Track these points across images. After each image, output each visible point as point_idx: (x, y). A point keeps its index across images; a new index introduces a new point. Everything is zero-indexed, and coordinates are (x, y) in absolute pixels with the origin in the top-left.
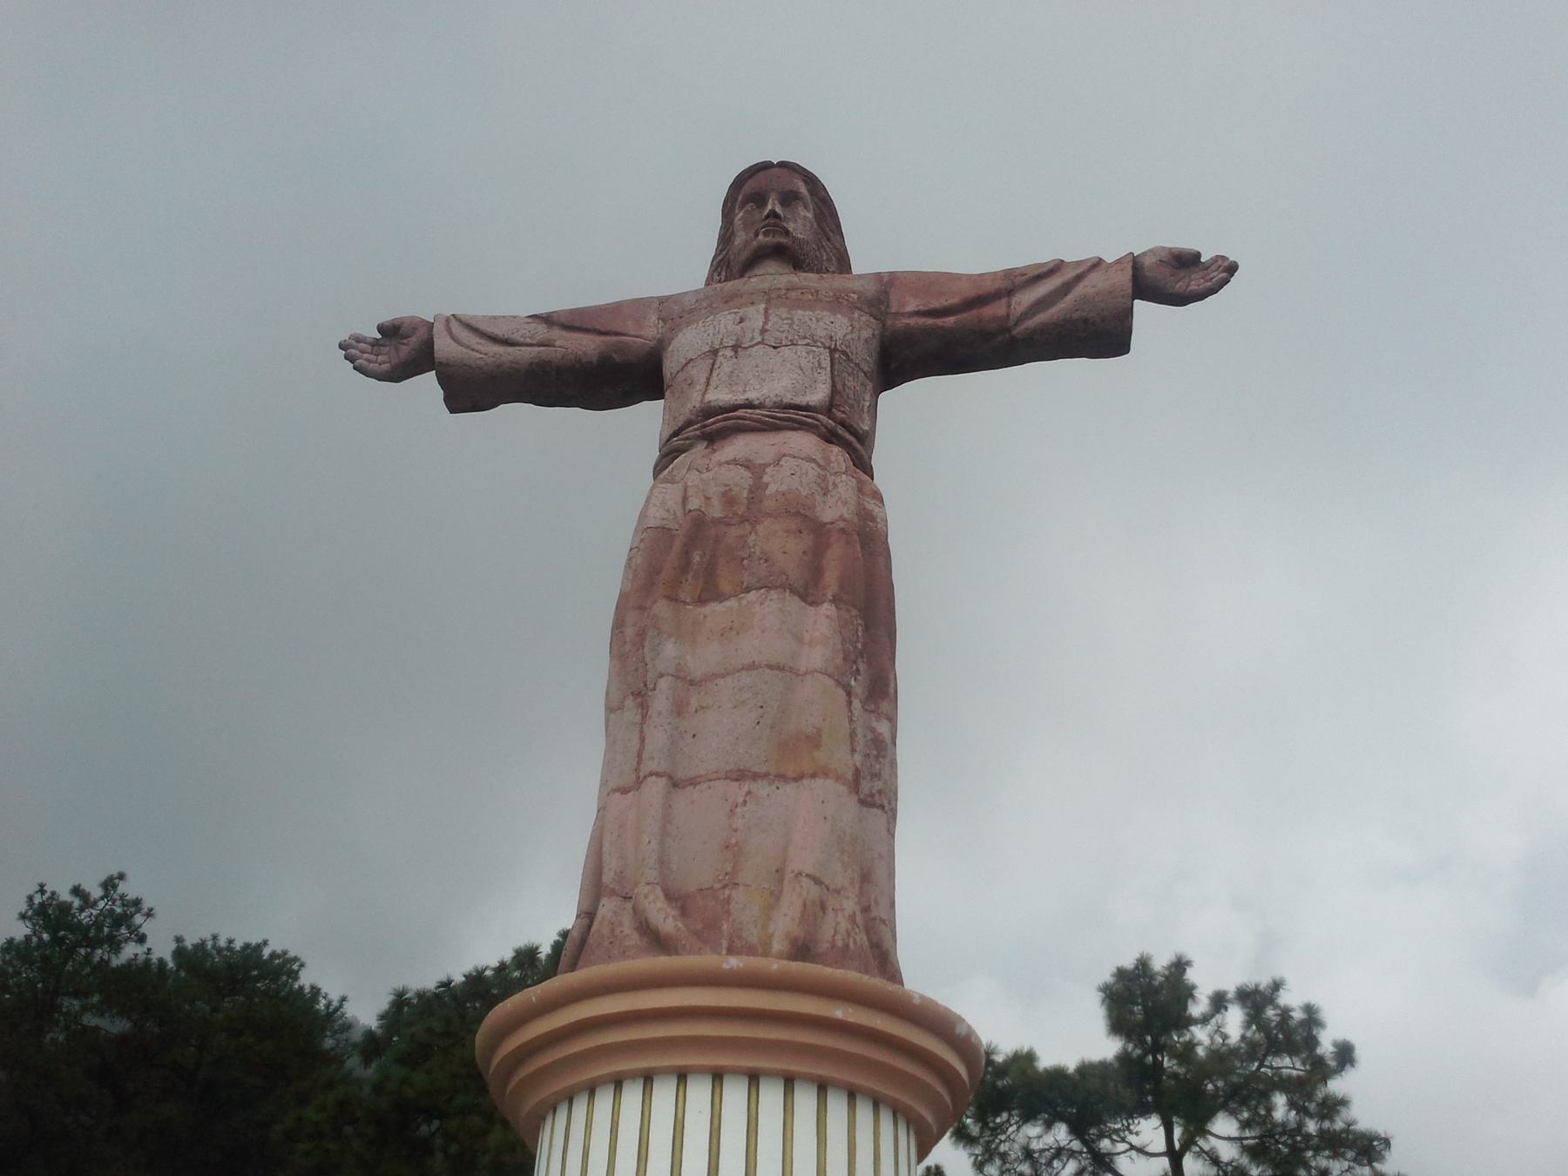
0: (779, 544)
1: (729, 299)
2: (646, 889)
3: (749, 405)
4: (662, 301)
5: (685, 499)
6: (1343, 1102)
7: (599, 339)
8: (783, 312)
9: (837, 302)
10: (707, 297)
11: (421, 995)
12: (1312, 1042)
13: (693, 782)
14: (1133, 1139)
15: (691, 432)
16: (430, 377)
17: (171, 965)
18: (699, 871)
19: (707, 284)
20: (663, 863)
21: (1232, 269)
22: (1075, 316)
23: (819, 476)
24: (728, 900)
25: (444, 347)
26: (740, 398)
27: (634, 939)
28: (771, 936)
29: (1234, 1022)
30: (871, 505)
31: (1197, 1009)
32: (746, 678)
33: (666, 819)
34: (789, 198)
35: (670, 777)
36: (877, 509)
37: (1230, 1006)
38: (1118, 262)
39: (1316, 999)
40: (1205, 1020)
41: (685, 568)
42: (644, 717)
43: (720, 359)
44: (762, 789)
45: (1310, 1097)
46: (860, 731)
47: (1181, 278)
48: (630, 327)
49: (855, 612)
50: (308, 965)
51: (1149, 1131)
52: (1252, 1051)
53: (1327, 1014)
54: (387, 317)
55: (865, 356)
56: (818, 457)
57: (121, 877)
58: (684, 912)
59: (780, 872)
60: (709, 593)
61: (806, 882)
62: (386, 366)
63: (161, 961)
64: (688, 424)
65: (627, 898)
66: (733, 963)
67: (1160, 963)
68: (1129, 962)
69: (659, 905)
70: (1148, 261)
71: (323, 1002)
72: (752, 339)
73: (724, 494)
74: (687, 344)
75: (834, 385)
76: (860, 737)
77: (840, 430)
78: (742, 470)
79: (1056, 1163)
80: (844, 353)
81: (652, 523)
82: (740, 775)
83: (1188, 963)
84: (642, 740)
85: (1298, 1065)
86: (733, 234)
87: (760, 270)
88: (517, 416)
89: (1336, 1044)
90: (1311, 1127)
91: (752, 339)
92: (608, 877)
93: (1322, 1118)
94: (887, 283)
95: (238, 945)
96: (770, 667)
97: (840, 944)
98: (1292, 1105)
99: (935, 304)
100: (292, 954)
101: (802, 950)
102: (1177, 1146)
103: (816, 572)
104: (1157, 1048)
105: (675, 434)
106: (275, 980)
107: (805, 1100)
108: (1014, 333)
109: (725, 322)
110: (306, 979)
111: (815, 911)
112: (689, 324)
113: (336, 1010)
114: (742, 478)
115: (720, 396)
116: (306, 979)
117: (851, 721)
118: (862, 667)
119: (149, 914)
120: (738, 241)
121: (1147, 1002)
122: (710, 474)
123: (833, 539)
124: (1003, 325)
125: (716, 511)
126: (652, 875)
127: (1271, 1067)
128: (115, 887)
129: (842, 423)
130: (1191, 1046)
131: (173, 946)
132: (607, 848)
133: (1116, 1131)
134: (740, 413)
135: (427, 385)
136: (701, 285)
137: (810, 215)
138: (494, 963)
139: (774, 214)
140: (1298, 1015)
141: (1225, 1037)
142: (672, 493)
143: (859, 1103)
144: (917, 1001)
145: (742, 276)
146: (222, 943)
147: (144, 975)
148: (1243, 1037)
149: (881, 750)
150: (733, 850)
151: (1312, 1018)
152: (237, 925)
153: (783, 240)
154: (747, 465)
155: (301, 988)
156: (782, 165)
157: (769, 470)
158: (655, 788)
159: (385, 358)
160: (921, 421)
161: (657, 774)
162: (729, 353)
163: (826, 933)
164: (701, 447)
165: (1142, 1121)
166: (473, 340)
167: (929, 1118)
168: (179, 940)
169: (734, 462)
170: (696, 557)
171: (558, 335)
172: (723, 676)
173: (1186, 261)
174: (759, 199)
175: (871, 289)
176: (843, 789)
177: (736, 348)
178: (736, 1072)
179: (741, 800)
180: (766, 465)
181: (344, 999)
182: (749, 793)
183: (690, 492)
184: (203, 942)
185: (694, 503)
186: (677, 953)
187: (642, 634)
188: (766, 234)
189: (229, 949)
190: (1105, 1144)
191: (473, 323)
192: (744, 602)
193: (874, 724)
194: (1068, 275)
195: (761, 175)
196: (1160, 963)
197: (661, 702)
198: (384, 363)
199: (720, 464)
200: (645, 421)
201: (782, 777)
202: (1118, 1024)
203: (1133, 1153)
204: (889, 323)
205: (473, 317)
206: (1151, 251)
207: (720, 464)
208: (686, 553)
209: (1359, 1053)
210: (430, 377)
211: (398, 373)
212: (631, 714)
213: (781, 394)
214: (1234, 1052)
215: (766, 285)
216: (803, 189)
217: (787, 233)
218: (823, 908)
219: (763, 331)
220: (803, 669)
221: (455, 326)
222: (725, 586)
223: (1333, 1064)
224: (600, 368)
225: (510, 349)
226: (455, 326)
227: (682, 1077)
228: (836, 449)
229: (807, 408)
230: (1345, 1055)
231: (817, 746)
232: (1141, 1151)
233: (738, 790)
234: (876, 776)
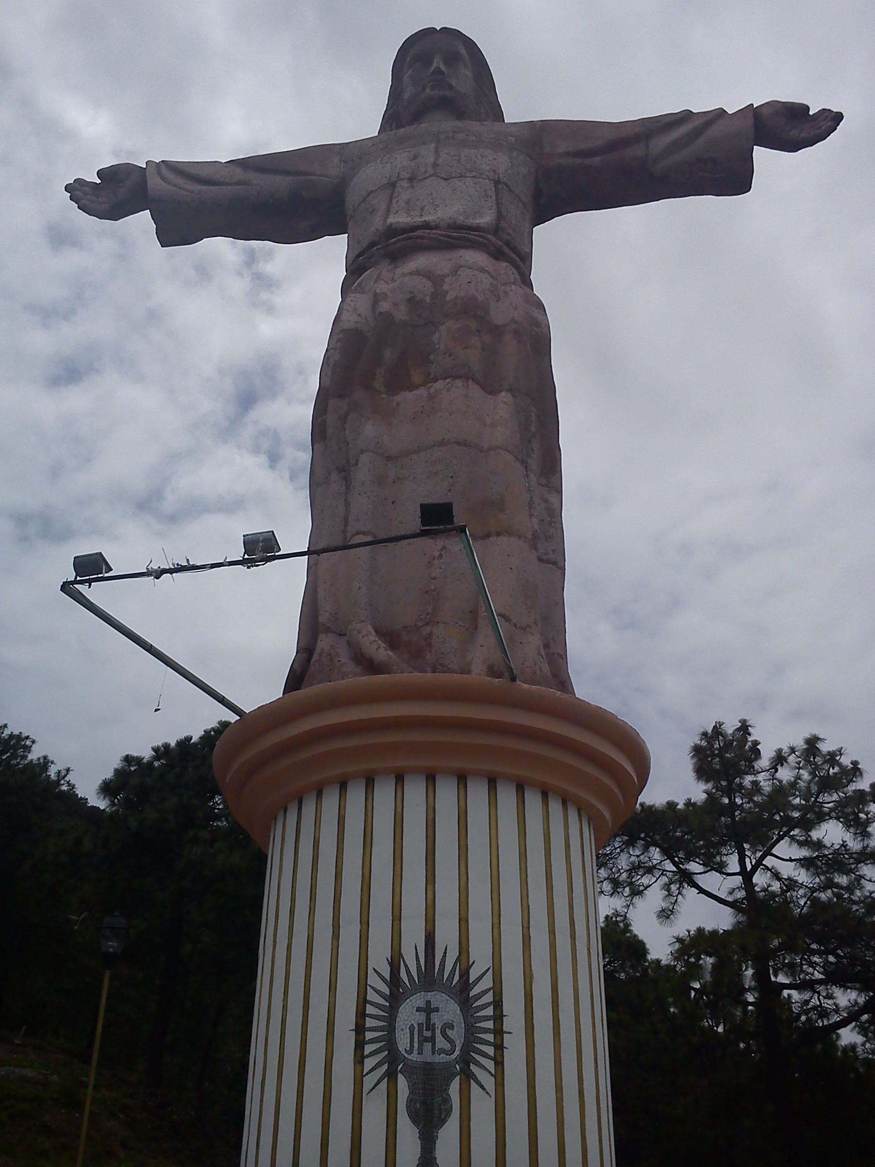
2: (359, 626)
3: (426, 226)
21: (838, 118)
23: (491, 285)
24: (431, 634)
25: (154, 183)
26: (418, 220)
27: (351, 667)
30: (536, 313)
31: (764, 762)
34: (452, 58)
36: (541, 318)
47: (795, 126)
64: (372, 244)
65: (341, 635)
67: (730, 727)
69: (372, 638)
72: (426, 172)
77: (506, 250)
78: (424, 280)
81: (346, 326)
92: (323, 618)
94: (540, 133)
96: (458, 443)
99: (583, 146)
100: (25, 734)
102: (749, 867)
104: (729, 792)
105: (358, 256)
107: (507, 797)
109: (401, 160)
115: (400, 219)
120: (406, 96)
121: (723, 755)
125: (402, 314)
129: (508, 244)
132: (321, 593)
134: (419, 233)
137: (469, 74)
139: (438, 71)
142: (362, 302)
162: (405, 184)
166: (181, 181)
171: (251, 176)
172: (416, 452)
173: (796, 113)
174: (425, 60)
177: (411, 180)
179: (437, 554)
180: (444, 276)
182: (444, 548)
185: (384, 306)
192: (432, 390)
194: (698, 122)
196: (730, 727)
197: (363, 474)
199: (404, 275)
202: (702, 772)
211: (115, 211)
213: (443, 231)
216: (463, 52)
217: (451, 87)
219: (435, 165)
221: (164, 170)
225: (213, 188)
226: (164, 170)
229: (477, 229)
234: (548, 538)
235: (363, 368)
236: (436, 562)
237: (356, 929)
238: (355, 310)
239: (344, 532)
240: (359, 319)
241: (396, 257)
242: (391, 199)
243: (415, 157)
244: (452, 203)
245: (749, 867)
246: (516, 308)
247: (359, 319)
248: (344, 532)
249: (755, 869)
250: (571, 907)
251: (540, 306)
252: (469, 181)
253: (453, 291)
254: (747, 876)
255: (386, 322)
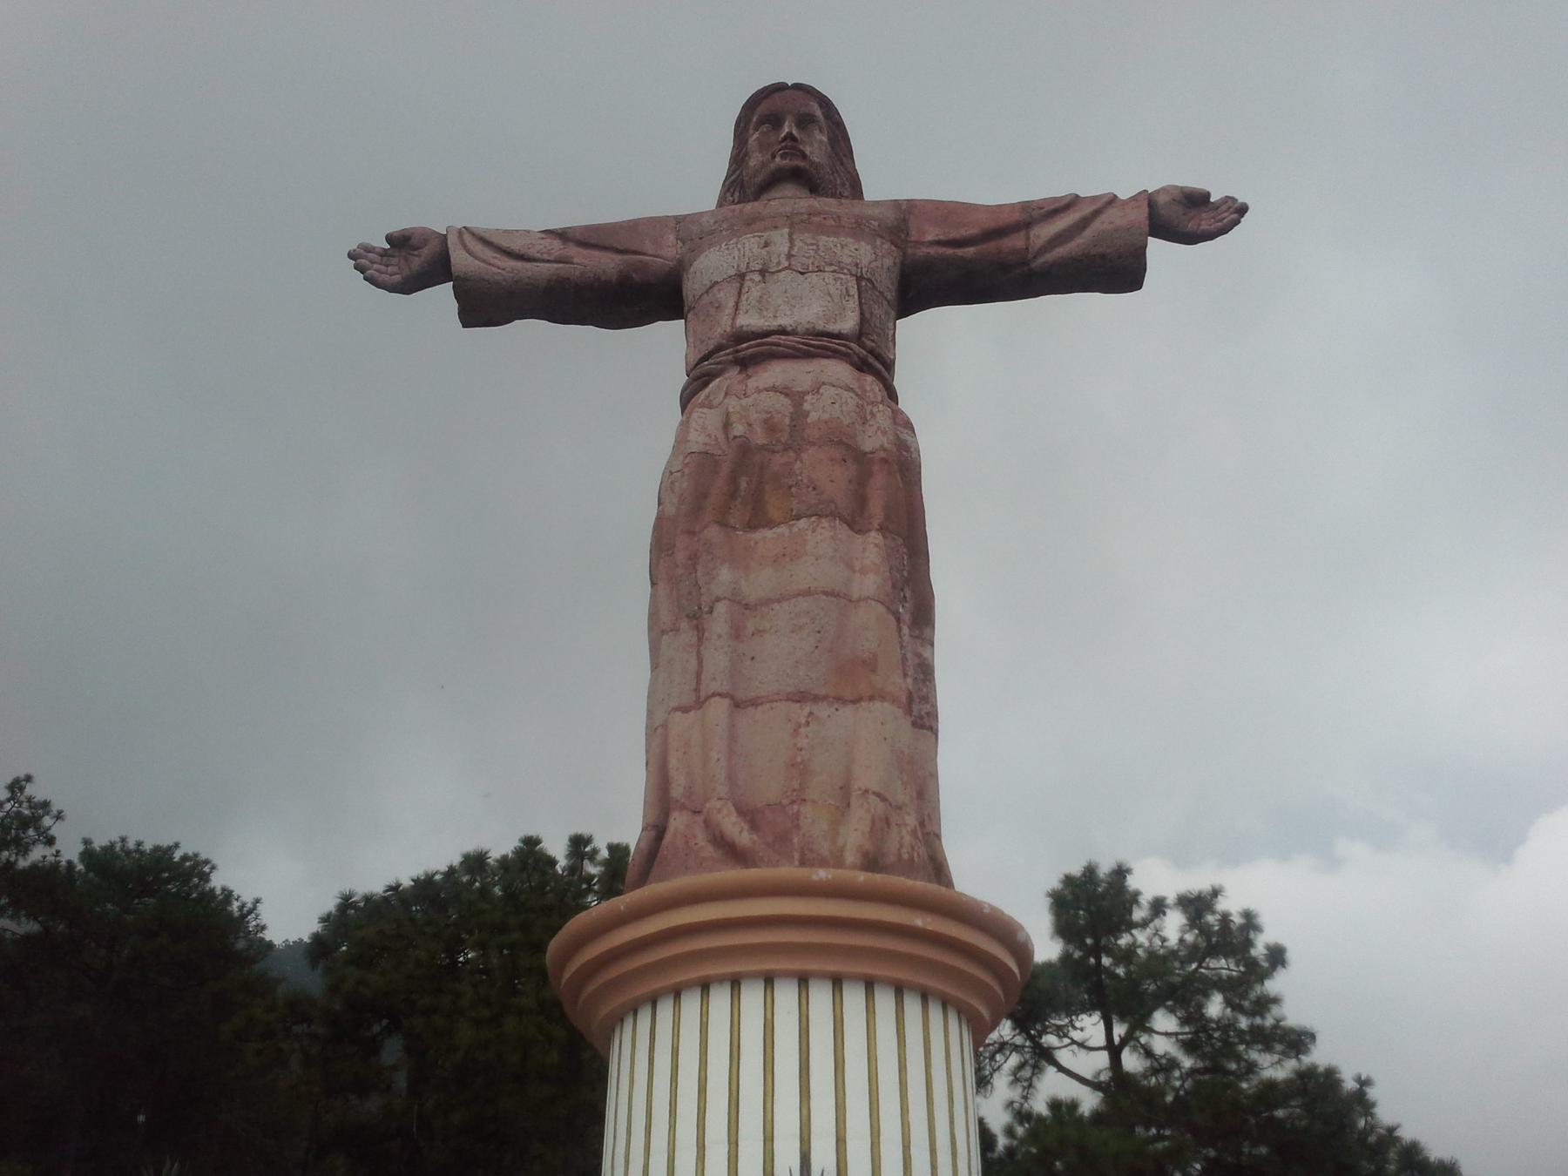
0: (822, 471)
1: (751, 222)
2: (719, 804)
3: (782, 331)
4: (679, 220)
5: (727, 426)
6: (1276, 1001)
7: (618, 258)
8: (808, 238)
9: (858, 229)
10: (725, 219)
11: (368, 899)
12: (1249, 943)
13: (755, 703)
14: (1076, 1035)
15: (722, 356)
16: (448, 287)
17: (80, 867)
18: (769, 788)
19: (720, 205)
20: (731, 779)
21: (1243, 210)
22: (1093, 252)
24: (798, 814)
25: (460, 260)
26: (774, 324)
27: (709, 851)
28: (842, 850)
29: (1173, 926)
30: (905, 436)
31: (1138, 914)
32: (803, 604)
33: (732, 738)
34: (805, 121)
35: (732, 698)
36: (909, 439)
37: (1168, 911)
38: (1134, 199)
39: (1253, 906)
40: (1144, 924)
41: (733, 495)
42: (700, 639)
43: (748, 283)
44: (823, 710)
45: (1244, 996)
46: (909, 656)
47: (1193, 217)
48: (648, 247)
49: (900, 541)
50: (220, 867)
51: (1090, 1027)
52: (1195, 953)
53: (1264, 920)
54: (396, 227)
55: (887, 284)
56: (855, 386)
57: (29, 779)
58: (754, 826)
59: (845, 790)
60: (758, 519)
61: (872, 798)
62: (397, 278)
63: (70, 863)
64: (719, 348)
65: (697, 812)
66: (822, 874)
68: (1076, 870)
70: (1162, 199)
71: (236, 905)
72: (779, 263)
73: (766, 421)
74: (711, 265)
75: (862, 314)
76: (910, 663)
77: (871, 360)
78: (782, 398)
79: (998, 1057)
80: (869, 280)
82: (801, 697)
83: (1129, 871)
84: (700, 661)
85: (1232, 966)
86: (747, 154)
87: (775, 193)
88: (530, 332)
89: (1268, 947)
90: (1244, 1023)
91: (779, 263)
92: (677, 791)
93: (1251, 1014)
94: (905, 215)
95: (148, 847)
96: (826, 593)
97: (906, 856)
98: (1228, 1002)
99: (954, 234)
100: (203, 856)
101: (872, 863)
102: (1117, 1040)
103: (862, 501)
104: (1097, 951)
105: (705, 358)
106: (186, 881)
108: (1033, 265)
109: (750, 245)
110: (217, 882)
111: (881, 826)
112: (710, 245)
113: (250, 912)
114: (782, 404)
115: (750, 320)
116: (217, 882)
117: (902, 647)
118: (908, 594)
119: (59, 816)
120: (752, 163)
121: (1093, 904)
122: (750, 400)
123: (876, 468)
124: (1023, 259)
125: (759, 438)
126: (722, 790)
127: (1207, 968)
128: (22, 789)
129: (871, 352)
130: (1133, 947)
131: (81, 848)
132: (673, 763)
133: (1059, 1028)
135: (442, 297)
136: (713, 206)
137: (825, 139)
138: (444, 868)
139: (790, 136)
140: (1237, 920)
141: (1164, 940)
143: (931, 1005)
144: (986, 911)
145: (756, 199)
146: (131, 845)
147: (50, 879)
148: (1181, 941)
149: (925, 672)
150: (799, 769)
151: (1251, 922)
152: (146, 827)
153: (802, 164)
154: (786, 392)
155: (213, 890)
156: (798, 87)
157: (808, 398)
158: (718, 710)
159: (395, 269)
160: (943, 352)
161: (720, 695)
162: (757, 277)
163: (892, 846)
164: (733, 372)
165: (1084, 1016)
166: (488, 254)
167: (985, 1013)
168: (87, 842)
169: (774, 389)
170: (743, 485)
171: (572, 250)
172: (779, 601)
173: (1196, 200)
174: (775, 121)
175: (890, 216)
176: (900, 712)
177: (763, 272)
178: (787, 974)
181: (257, 901)
182: (811, 714)
183: (734, 418)
184: (112, 845)
185: (738, 429)
186: (755, 865)
187: (694, 559)
188: (783, 157)
189: (137, 851)
190: (1050, 1040)
191: (487, 236)
192: (795, 529)
193: (920, 650)
194: (1087, 210)
195: (776, 96)
197: (719, 624)
198: (395, 274)
199: (759, 391)
200: (663, 346)
201: (840, 700)
203: (1075, 1047)
204: (910, 251)
205: (486, 231)
206: (1163, 189)
207: (759, 391)
208: (734, 480)
209: (1290, 955)
210: (448, 287)
211: (409, 286)
212: (687, 636)
213: (793, 313)
214: (1173, 953)
215: (788, 209)
216: (819, 113)
217: (804, 157)
218: (888, 824)
219: (789, 256)
220: (855, 596)
221: (467, 237)
222: (774, 513)
223: (1266, 965)
224: (615, 286)
225: (528, 265)
226: (467, 237)
227: (769, 980)
228: (870, 378)
229: (839, 336)
230: (1277, 956)
231: (873, 671)
232: (1082, 1045)
233: (800, 712)
235: (718, 501)
236: (802, 730)
237: (723, 1149)
238: (704, 428)
239: (697, 690)
240: (707, 440)
241: (746, 364)
242: (740, 293)
243: (766, 245)
244: (814, 302)
245: (1117, 1040)
246: (884, 433)
247: (707, 440)
248: (697, 690)
249: (1124, 1041)
250: (952, 1122)
251: (909, 426)
252: (829, 277)
253: (819, 410)
254: (1114, 1051)
255: (745, 449)
